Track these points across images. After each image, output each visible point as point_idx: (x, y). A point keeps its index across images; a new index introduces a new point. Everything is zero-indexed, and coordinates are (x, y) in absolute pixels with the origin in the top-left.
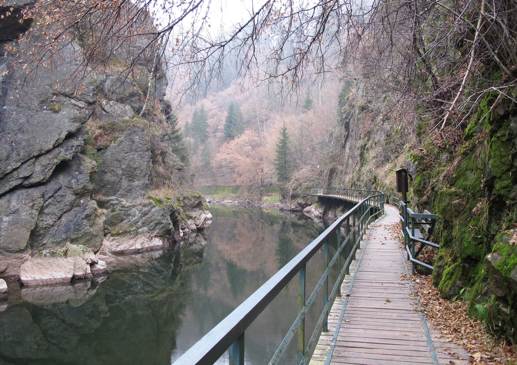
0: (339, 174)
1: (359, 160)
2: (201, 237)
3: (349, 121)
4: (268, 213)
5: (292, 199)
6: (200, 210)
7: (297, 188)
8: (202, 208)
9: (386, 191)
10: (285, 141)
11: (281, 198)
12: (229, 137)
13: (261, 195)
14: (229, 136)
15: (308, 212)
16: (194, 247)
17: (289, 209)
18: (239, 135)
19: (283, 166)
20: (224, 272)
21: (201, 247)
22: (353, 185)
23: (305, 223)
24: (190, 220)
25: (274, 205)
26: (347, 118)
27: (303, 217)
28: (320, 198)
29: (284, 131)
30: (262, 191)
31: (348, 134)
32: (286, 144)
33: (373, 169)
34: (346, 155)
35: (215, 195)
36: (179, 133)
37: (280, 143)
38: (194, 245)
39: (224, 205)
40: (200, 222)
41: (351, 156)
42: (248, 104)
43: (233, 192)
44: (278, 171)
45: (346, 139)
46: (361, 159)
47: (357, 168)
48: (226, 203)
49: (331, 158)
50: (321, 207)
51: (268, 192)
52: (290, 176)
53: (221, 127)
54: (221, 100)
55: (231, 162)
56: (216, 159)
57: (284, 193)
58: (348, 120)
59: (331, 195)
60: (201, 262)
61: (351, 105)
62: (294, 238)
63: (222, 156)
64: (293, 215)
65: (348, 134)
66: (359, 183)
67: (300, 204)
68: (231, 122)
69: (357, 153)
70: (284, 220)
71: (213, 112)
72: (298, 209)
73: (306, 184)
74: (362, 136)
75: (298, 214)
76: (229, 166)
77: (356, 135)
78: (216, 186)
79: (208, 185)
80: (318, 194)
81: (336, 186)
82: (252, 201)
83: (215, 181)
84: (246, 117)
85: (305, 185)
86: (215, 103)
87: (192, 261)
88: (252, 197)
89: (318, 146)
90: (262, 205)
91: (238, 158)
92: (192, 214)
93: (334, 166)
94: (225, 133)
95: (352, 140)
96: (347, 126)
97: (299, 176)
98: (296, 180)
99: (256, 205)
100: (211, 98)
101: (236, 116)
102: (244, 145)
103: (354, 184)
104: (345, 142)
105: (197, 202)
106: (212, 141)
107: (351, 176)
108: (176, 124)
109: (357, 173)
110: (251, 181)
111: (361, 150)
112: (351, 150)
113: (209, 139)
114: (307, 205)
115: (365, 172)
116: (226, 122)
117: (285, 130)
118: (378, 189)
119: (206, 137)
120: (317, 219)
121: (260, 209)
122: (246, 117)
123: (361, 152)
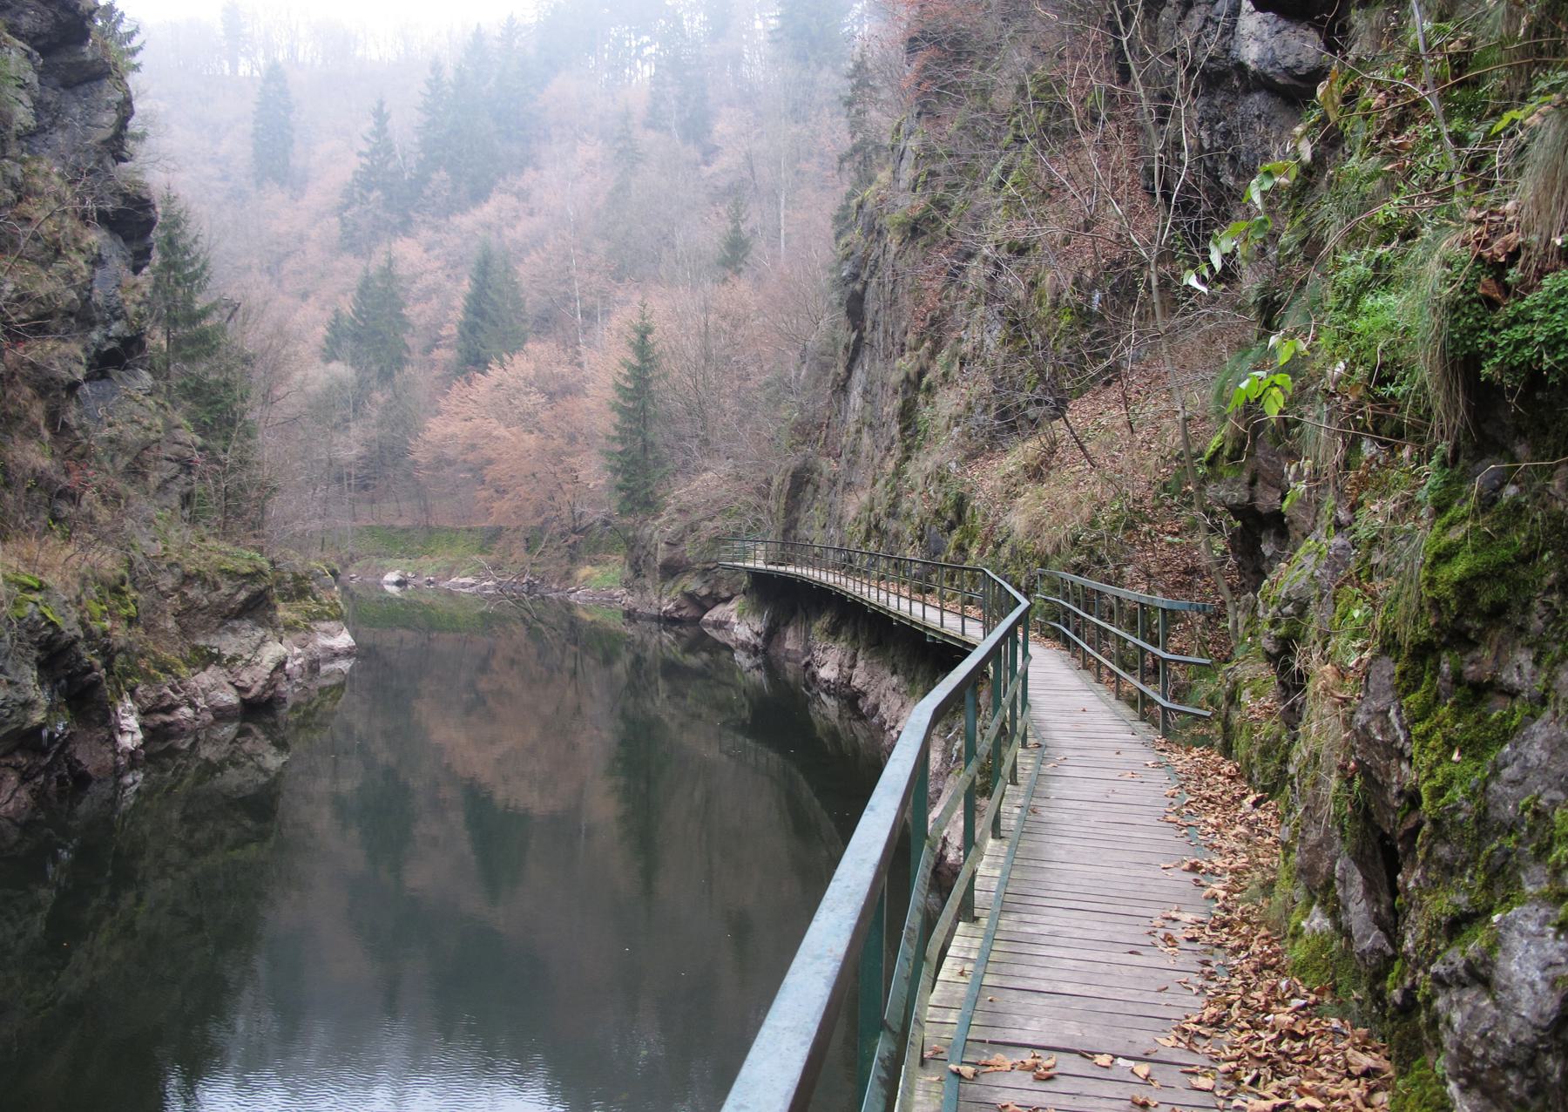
0: (824, 490)
1: (898, 436)
2: (262, 737)
3: (864, 289)
4: (593, 622)
5: (664, 579)
6: (262, 625)
7: (681, 540)
8: (271, 620)
9: (1012, 566)
10: (645, 372)
11: (629, 574)
12: (475, 364)
13: (573, 559)
14: (474, 361)
15: (720, 625)
16: (232, 778)
17: (654, 612)
18: (506, 357)
19: (634, 462)
20: (457, 818)
21: (262, 779)
22: (874, 533)
23: (706, 665)
24: (210, 670)
25: (610, 596)
26: (855, 277)
27: (700, 642)
28: (758, 578)
29: (644, 337)
30: (574, 546)
31: (860, 339)
32: (647, 382)
33: (953, 465)
34: (852, 418)
35: (422, 560)
36: (208, 323)
37: (626, 378)
38: (231, 770)
39: (450, 593)
40: (255, 678)
41: (868, 421)
42: (543, 255)
43: (482, 551)
44: (619, 478)
45: (852, 360)
46: (903, 431)
47: (890, 465)
48: (456, 585)
49: (795, 429)
50: (757, 610)
51: (596, 548)
52: (662, 497)
53: (450, 330)
54: (458, 241)
55: (473, 447)
56: (428, 436)
57: (638, 558)
58: (858, 287)
59: (791, 569)
60: (262, 837)
61: (871, 231)
62: (672, 717)
63: (446, 425)
64: (667, 637)
65: (860, 339)
66: (892, 525)
67: (691, 597)
68: (481, 314)
69: (892, 406)
70: (638, 650)
71: (429, 280)
72: (683, 613)
73: (711, 525)
74: (911, 339)
75: (684, 631)
76: (465, 461)
77: (889, 340)
78: (428, 526)
79: (400, 524)
80: (750, 564)
81: (812, 535)
82: (543, 580)
83: (426, 510)
84: (533, 300)
85: (708, 529)
86: (437, 251)
87: (222, 836)
88: (543, 569)
89: (762, 396)
90: (572, 596)
91: (495, 433)
92: (223, 645)
93: (806, 458)
94: (460, 351)
95: (873, 360)
96: (855, 308)
97: (690, 498)
98: (680, 511)
99: (553, 595)
100: (425, 234)
101: (500, 292)
102: (519, 390)
103: (876, 526)
104: (849, 370)
105: (243, 596)
106: (414, 372)
107: (864, 497)
108: (201, 289)
109: (887, 484)
110: (539, 512)
111: (905, 392)
112: (869, 398)
113: (408, 369)
114: (716, 600)
115: (920, 481)
116: (465, 315)
117: (644, 332)
118: (974, 552)
119: (400, 362)
120: (744, 654)
121: (568, 609)
122: (533, 300)
123: (905, 402)
